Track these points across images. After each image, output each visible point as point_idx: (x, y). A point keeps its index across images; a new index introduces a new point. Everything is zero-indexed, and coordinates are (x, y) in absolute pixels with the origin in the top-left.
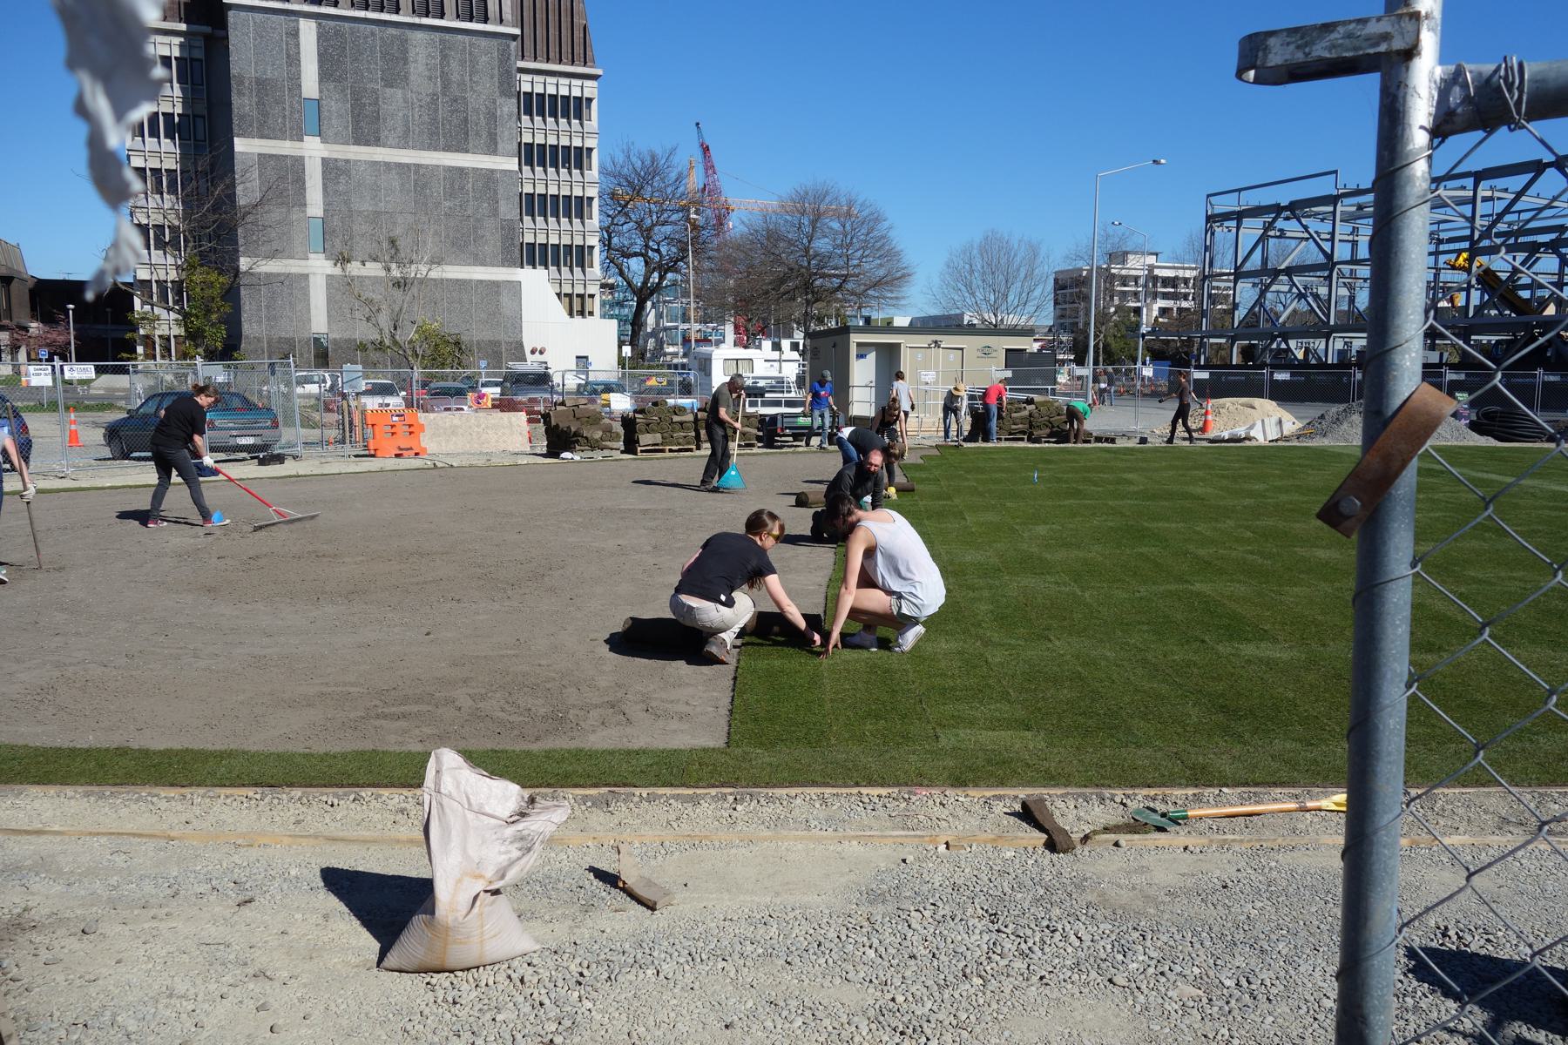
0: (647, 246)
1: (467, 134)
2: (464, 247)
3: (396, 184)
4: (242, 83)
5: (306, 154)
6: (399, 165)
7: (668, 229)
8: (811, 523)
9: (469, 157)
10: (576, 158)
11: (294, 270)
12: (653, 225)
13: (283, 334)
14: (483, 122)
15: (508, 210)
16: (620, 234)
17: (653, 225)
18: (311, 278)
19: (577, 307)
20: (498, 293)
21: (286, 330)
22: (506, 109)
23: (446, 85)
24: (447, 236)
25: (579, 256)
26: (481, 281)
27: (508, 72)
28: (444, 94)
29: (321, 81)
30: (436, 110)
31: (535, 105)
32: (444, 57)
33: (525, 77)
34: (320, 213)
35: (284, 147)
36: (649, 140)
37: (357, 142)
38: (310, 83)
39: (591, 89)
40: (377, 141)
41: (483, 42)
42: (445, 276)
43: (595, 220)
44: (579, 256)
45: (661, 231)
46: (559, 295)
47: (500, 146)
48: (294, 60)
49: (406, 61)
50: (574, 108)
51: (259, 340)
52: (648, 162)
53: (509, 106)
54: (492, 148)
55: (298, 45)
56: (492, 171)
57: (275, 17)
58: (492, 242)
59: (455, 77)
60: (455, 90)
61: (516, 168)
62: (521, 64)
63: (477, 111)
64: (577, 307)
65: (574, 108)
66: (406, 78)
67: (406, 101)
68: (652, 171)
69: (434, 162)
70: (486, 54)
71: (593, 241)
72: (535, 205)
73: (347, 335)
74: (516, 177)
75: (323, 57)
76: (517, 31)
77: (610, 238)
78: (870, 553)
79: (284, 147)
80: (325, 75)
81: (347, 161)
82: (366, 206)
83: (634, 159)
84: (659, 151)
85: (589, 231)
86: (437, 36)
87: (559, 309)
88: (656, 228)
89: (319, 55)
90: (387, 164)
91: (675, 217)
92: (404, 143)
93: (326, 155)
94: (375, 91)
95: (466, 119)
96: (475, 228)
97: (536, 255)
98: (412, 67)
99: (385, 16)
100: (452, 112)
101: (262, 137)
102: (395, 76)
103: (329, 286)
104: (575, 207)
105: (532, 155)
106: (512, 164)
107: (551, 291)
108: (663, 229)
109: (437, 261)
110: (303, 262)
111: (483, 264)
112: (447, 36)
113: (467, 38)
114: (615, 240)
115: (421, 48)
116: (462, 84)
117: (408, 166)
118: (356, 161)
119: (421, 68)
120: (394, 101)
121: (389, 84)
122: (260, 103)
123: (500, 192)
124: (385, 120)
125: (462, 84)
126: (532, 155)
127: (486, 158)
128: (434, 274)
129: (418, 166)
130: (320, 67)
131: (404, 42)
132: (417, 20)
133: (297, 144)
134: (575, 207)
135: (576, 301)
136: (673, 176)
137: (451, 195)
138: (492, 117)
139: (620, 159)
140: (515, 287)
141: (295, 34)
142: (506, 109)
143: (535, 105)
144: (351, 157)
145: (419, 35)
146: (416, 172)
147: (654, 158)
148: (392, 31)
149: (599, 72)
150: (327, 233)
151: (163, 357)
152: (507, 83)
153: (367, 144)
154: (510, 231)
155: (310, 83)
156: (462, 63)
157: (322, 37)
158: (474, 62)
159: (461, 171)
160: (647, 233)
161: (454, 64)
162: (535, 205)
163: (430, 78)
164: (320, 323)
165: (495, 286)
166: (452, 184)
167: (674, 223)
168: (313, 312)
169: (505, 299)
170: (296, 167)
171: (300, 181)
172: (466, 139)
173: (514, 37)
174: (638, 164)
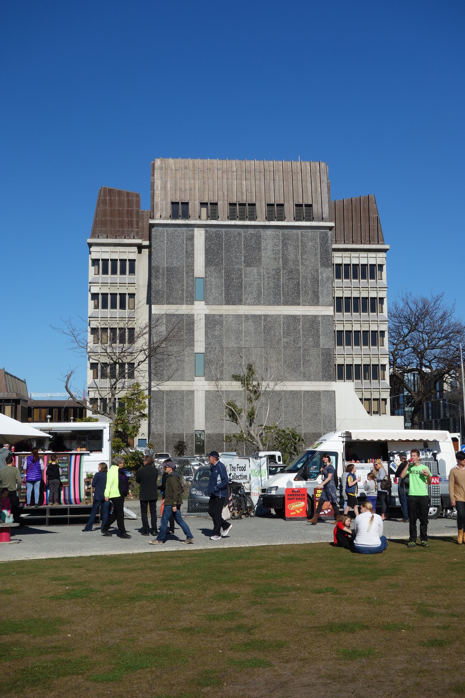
0: (421, 364)
1: (299, 293)
2: (296, 369)
3: (252, 329)
4: (158, 271)
5: (195, 313)
6: (254, 316)
7: (437, 351)
8: (428, 526)
9: (286, 313)
10: (372, 305)
11: (184, 388)
12: (426, 349)
13: (176, 432)
14: (309, 284)
15: (326, 341)
16: (402, 357)
17: (426, 349)
18: (196, 393)
19: (375, 408)
20: (319, 400)
21: (180, 429)
22: (325, 275)
23: (285, 262)
24: (285, 362)
25: (373, 371)
26: (308, 392)
27: (327, 251)
28: (284, 268)
29: (206, 266)
30: (279, 279)
31: (343, 271)
32: (285, 245)
33: (336, 254)
34: (202, 350)
35: (183, 309)
36: (422, 290)
37: (228, 303)
38: (199, 267)
39: (380, 258)
40: (240, 302)
41: (310, 233)
42: (284, 389)
43: (386, 347)
44: (373, 371)
45: (430, 354)
46: (361, 399)
47: (320, 300)
48: (190, 254)
49: (260, 250)
50: (371, 271)
51: (161, 436)
52: (421, 306)
53: (329, 272)
54: (315, 302)
55: (193, 245)
56: (316, 317)
57: (179, 229)
58: (316, 363)
59: (291, 257)
60: (291, 265)
61: (332, 313)
62: (334, 246)
63: (305, 278)
64: (375, 408)
65: (371, 271)
66: (260, 260)
67: (259, 274)
68: (424, 313)
69: (277, 313)
70: (313, 243)
71: (385, 361)
72: (345, 338)
73: (217, 431)
74: (329, 319)
75: (208, 251)
76: (332, 224)
77: (395, 360)
78: (324, 481)
79: (183, 309)
80: (209, 262)
81: (221, 316)
82: (232, 344)
83: (411, 305)
84: (429, 298)
85: (381, 355)
86: (281, 232)
87: (361, 409)
88: (428, 351)
89: (206, 250)
90: (246, 316)
91: (441, 343)
92: (257, 302)
93: (207, 312)
94: (240, 270)
95: (298, 284)
96: (304, 355)
97: (346, 372)
98: (263, 253)
99: (247, 223)
100: (289, 279)
101: (168, 304)
102: (253, 260)
103: (207, 398)
104: (373, 338)
105: (342, 304)
106: (329, 311)
107: (356, 398)
108: (433, 351)
109: (280, 379)
110: (190, 383)
111: (308, 380)
112: (287, 231)
113: (299, 231)
114: (399, 361)
115: (269, 240)
116: (296, 261)
117: (260, 316)
118: (227, 315)
119: (269, 253)
120: (251, 275)
121: (248, 264)
122: (169, 282)
123: (321, 330)
124: (246, 287)
125: (296, 261)
126: (342, 304)
127: (312, 308)
128: (277, 388)
129: (266, 316)
130: (206, 257)
131: (259, 238)
132: (267, 223)
133: (190, 307)
134: (373, 338)
135: (374, 404)
136: (440, 314)
137: (287, 334)
138: (315, 280)
139: (401, 305)
140: (331, 395)
141: (191, 238)
142: (325, 275)
143: (343, 271)
144: (223, 312)
145: (269, 232)
146: (265, 320)
147: (425, 303)
148: (251, 231)
149: (387, 247)
150: (207, 363)
151: (120, 342)
152: (326, 260)
153: (234, 304)
154: (328, 356)
155: (199, 267)
156: (296, 247)
157: (208, 239)
158: (304, 246)
159: (295, 318)
160: (421, 355)
161: (290, 248)
162: (345, 338)
163: (275, 259)
164: (199, 423)
165: (317, 394)
166: (288, 327)
167: (441, 347)
168: (196, 416)
169: (324, 404)
170: (188, 322)
171: (191, 331)
172: (298, 296)
173: (330, 228)
174: (413, 307)
